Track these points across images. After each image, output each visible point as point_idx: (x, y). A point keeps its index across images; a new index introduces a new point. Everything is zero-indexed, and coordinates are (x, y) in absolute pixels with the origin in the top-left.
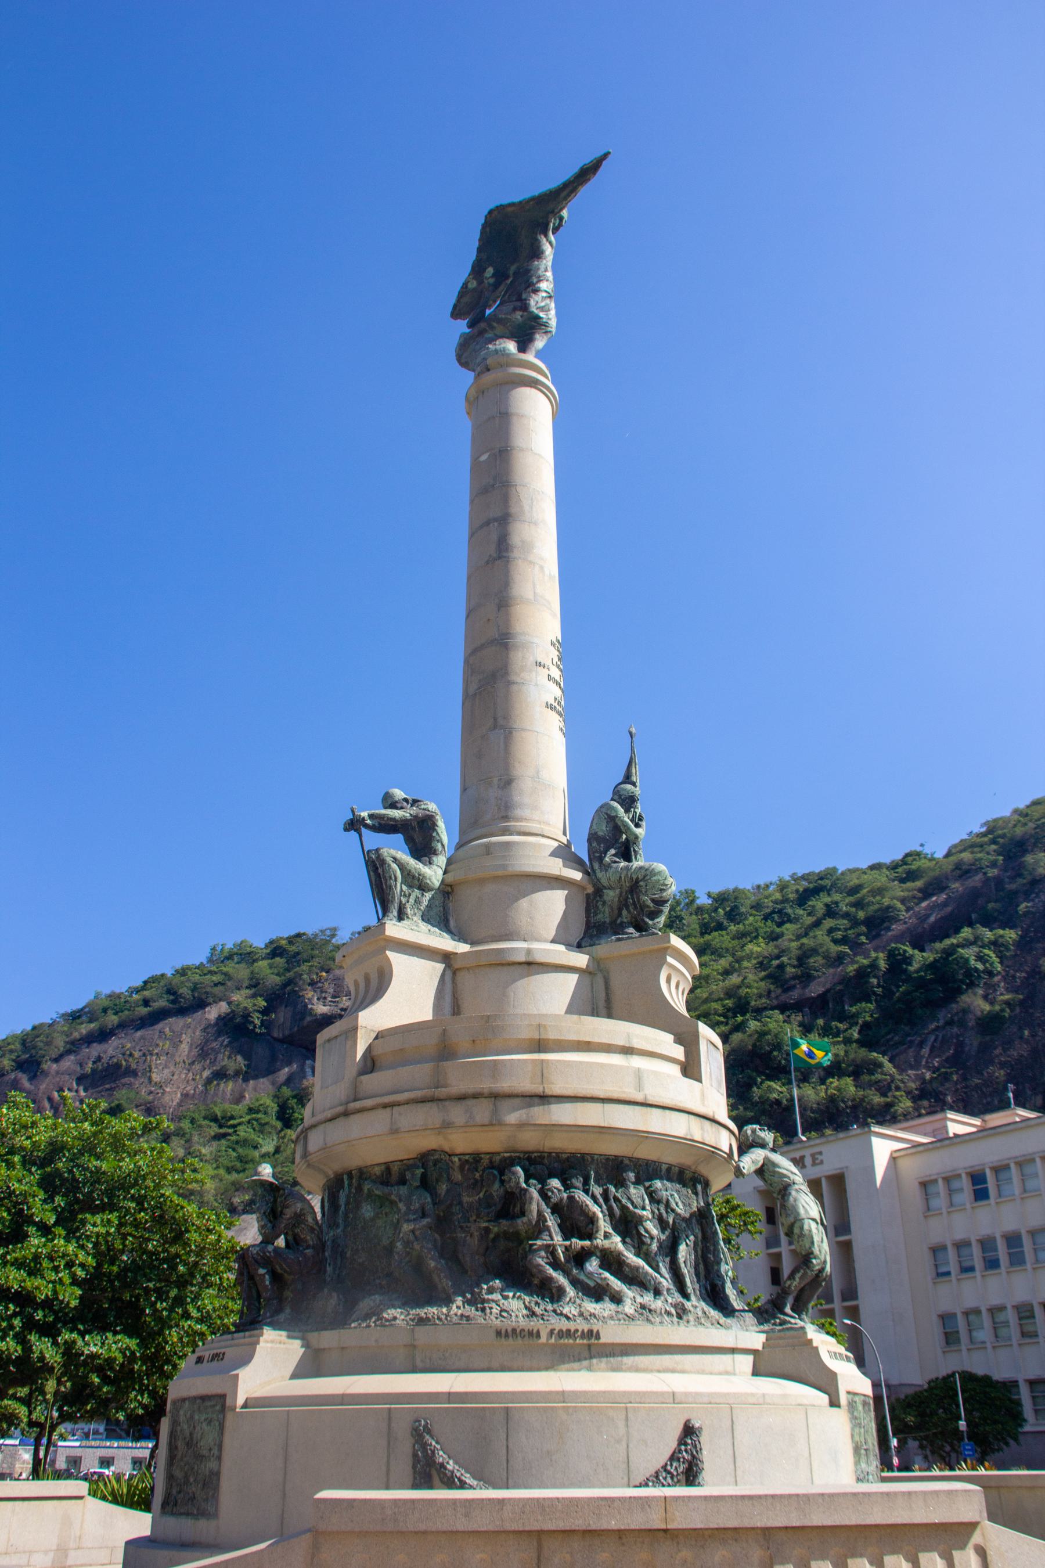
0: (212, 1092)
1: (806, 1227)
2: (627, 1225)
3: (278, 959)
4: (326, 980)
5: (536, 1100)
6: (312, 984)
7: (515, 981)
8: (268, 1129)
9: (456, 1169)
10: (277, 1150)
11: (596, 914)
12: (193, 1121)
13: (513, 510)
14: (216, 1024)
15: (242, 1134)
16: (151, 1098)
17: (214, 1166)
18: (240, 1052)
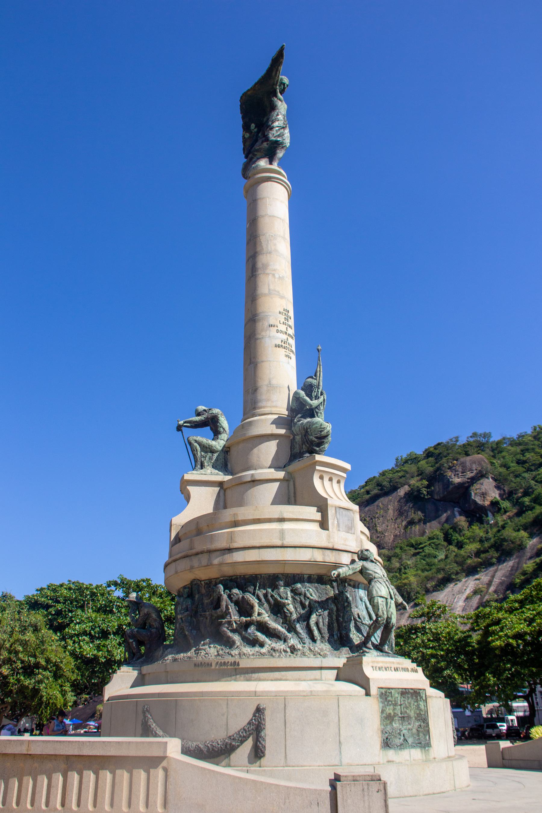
0: (409, 532)
1: (376, 601)
2: (277, 609)
3: (430, 459)
4: (457, 465)
5: (227, 551)
6: (450, 468)
7: (247, 491)
8: (440, 547)
9: (203, 587)
10: (447, 557)
11: (294, 449)
12: (401, 548)
13: (258, 249)
14: (404, 497)
15: (427, 551)
16: (378, 540)
17: (415, 569)
18: (419, 509)
